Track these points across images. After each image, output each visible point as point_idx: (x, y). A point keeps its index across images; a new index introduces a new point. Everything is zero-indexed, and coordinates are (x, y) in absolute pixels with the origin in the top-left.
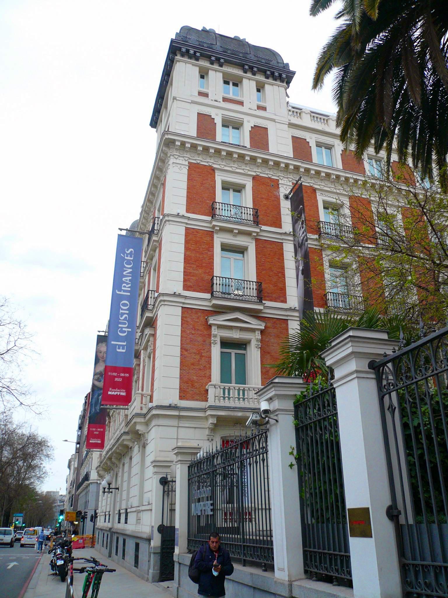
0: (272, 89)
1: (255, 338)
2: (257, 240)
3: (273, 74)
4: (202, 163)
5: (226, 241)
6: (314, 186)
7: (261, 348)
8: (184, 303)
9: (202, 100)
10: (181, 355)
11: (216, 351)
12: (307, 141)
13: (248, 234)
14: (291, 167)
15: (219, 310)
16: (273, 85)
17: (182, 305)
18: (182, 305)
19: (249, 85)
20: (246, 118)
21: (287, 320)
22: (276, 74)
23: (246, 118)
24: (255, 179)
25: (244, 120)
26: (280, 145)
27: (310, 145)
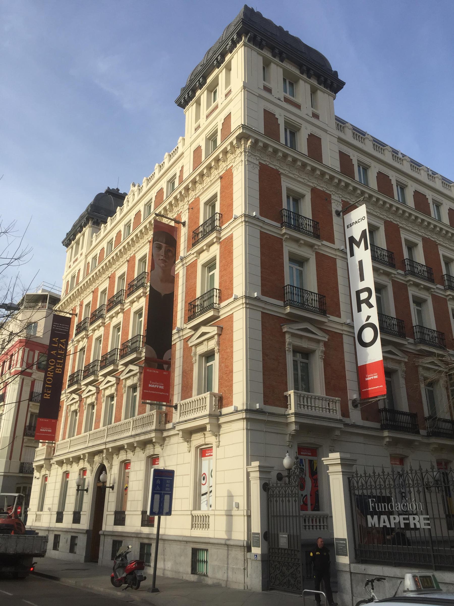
0: (322, 96)
1: (319, 350)
2: (317, 254)
3: (326, 80)
4: (270, 166)
5: (292, 250)
6: (279, 170)
7: (323, 359)
8: (264, 308)
9: (265, 94)
10: (263, 360)
11: (290, 358)
12: (276, 117)
13: (312, 246)
14: (261, 144)
15: (292, 319)
16: (324, 93)
17: (261, 310)
18: (261, 310)
19: (303, 88)
20: (304, 125)
21: (342, 334)
22: (329, 82)
23: (304, 125)
24: (314, 191)
25: (302, 126)
26: (330, 159)
27: (353, 163)
